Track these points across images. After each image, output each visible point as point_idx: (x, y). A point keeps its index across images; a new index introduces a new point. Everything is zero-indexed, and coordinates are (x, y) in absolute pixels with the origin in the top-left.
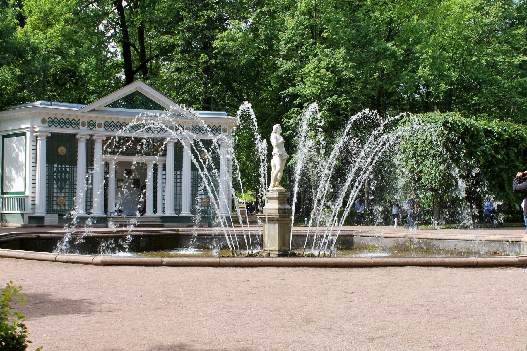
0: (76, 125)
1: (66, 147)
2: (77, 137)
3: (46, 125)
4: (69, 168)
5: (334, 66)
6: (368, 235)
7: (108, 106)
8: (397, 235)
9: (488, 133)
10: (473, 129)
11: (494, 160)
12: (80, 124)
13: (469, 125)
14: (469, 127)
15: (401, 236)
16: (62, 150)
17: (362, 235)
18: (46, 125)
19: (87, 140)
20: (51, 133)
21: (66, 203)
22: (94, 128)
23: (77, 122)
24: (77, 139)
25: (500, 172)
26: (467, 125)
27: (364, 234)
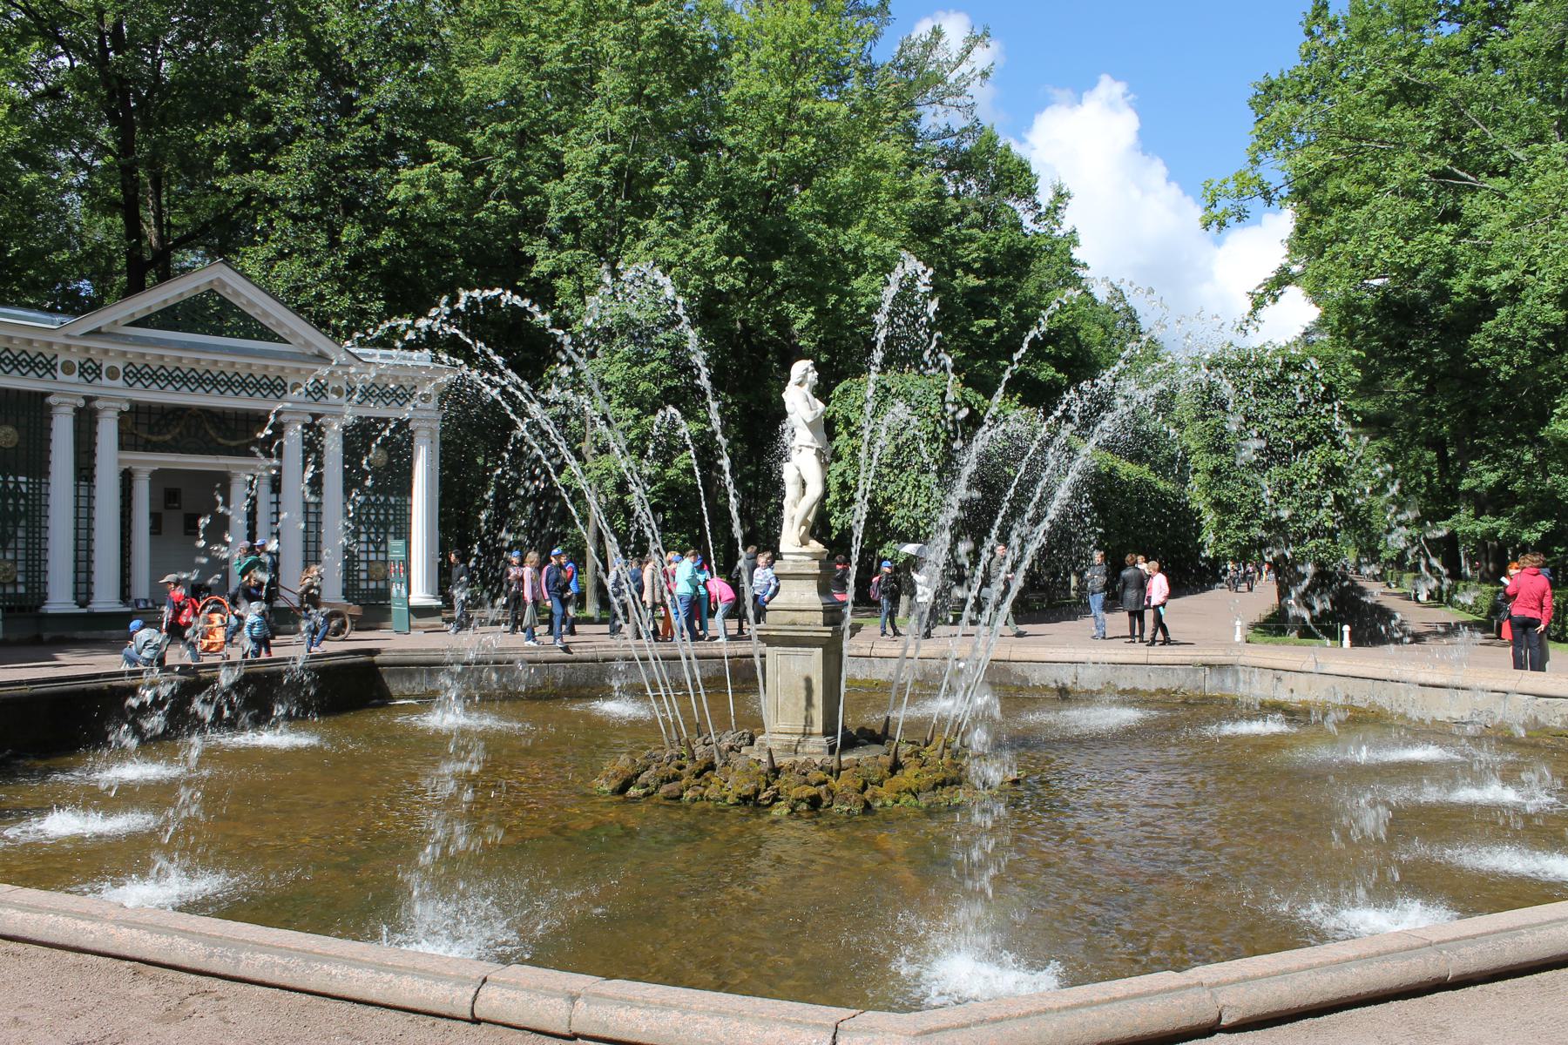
2: (51, 400)
4: (27, 483)
19: (78, 411)
21: (20, 579)
23: (49, 362)
24: (50, 407)
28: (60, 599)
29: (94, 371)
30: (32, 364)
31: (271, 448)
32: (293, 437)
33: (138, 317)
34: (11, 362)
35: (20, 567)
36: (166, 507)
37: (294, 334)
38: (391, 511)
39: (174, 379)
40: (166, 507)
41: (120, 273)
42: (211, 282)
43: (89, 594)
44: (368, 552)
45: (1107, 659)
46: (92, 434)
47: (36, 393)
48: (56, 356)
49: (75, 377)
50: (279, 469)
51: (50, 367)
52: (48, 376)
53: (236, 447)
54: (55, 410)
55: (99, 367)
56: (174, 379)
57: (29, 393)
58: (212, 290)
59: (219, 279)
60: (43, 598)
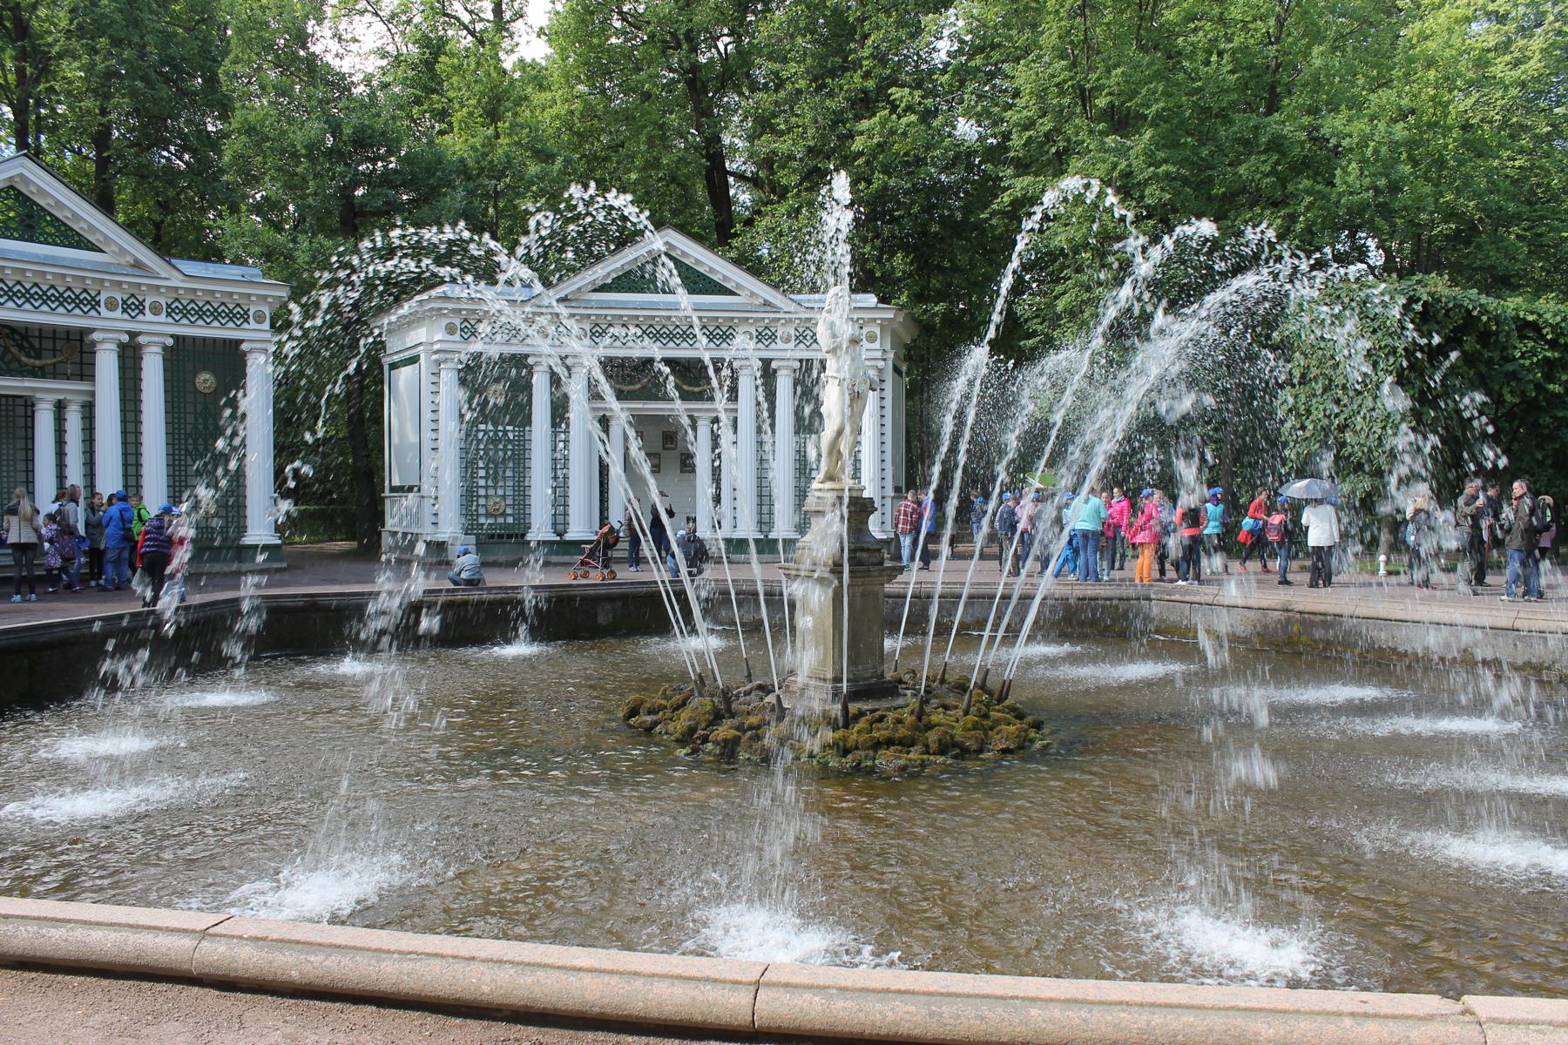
0: (93, 307)
1: (214, 373)
2: (244, 347)
3: (457, 337)
4: (513, 431)
5: (1127, 175)
6: (1188, 598)
7: (603, 288)
8: (1265, 604)
9: (1528, 329)
10: (1484, 318)
11: (1541, 398)
12: (102, 304)
13: (1475, 308)
14: (1475, 313)
15: (1273, 606)
16: (205, 380)
17: (1173, 598)
18: (457, 337)
19: (122, 347)
20: (175, 337)
21: (509, 511)
22: (245, 325)
23: (93, 298)
24: (244, 354)
25: (1558, 428)
26: (1471, 307)
27: (1177, 597)
28: (540, 529)
29: (137, 307)
30: (77, 302)
31: (85, 370)
32: (107, 365)
33: (600, 283)
34: (227, 315)
35: (509, 502)
36: (664, 448)
37: (739, 286)
38: (510, 447)
39: (235, 316)
40: (664, 448)
41: (123, 201)
42: (11, 178)
43: (566, 524)
44: (486, 487)
45: (1487, 622)
46: (138, 369)
47: (231, 341)
48: (99, 293)
49: (118, 313)
50: (93, 394)
51: (95, 304)
52: (93, 313)
53: (42, 368)
54: (99, 347)
55: (246, 312)
56: (204, 313)
57: (224, 340)
58: (12, 187)
59: (21, 175)
60: (242, 529)
